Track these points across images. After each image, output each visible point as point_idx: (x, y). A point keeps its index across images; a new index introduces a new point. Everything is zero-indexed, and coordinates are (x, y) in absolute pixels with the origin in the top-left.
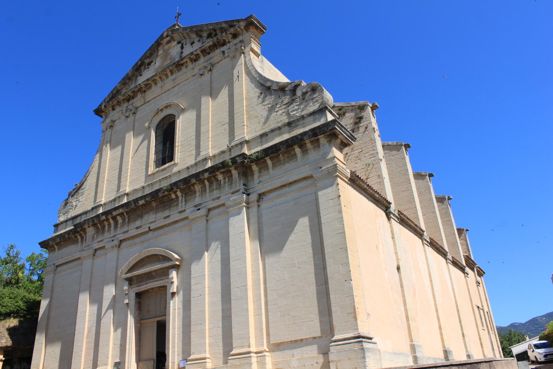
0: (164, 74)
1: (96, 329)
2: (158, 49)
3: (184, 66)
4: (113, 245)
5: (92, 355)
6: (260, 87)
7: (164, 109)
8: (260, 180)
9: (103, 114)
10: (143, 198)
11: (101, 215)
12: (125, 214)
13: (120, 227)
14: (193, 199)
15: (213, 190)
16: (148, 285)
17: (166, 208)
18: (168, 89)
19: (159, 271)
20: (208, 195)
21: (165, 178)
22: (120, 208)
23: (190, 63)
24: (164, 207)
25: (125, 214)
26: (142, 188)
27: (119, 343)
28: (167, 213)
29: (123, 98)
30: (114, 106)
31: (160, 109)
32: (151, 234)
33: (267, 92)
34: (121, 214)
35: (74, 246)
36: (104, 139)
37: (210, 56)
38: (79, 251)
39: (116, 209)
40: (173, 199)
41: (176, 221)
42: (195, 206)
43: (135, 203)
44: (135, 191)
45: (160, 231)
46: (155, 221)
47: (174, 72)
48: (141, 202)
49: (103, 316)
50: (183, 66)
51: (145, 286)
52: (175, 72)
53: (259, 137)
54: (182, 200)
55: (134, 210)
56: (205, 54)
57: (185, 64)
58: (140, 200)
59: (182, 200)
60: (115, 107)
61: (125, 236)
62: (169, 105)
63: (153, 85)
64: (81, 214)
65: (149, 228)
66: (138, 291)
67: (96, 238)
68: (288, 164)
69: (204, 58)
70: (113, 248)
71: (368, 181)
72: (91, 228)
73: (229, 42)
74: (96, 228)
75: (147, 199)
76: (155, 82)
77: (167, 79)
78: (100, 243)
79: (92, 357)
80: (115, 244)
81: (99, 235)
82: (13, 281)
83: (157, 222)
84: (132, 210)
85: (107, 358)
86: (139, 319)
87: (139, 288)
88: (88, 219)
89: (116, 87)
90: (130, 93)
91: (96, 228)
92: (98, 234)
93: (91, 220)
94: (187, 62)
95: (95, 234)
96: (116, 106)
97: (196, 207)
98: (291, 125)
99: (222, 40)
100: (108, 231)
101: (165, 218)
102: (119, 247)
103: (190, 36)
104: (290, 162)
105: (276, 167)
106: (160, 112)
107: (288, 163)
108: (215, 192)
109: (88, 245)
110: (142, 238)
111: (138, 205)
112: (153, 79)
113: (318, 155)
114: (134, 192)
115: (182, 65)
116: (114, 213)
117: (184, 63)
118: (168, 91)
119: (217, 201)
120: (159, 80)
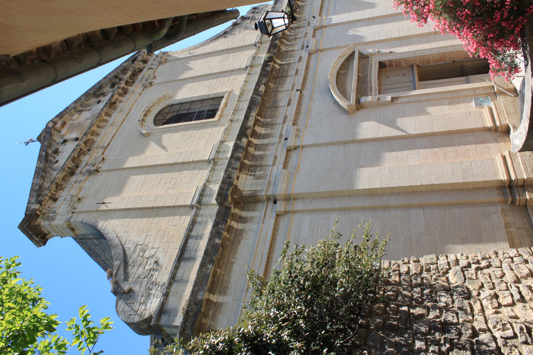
0: (101, 121)
1: (423, 149)
2: (52, 140)
3: (117, 103)
4: (295, 133)
5: (468, 146)
7: (145, 118)
9: (39, 220)
10: (259, 84)
11: (239, 142)
12: (259, 118)
16: (373, 80)
18: (122, 120)
19: (360, 69)
21: (241, 96)
22: (250, 113)
23: (121, 97)
25: (259, 118)
26: (231, 122)
27: (448, 106)
29: (62, 176)
30: (53, 196)
31: (141, 119)
32: (305, 92)
34: (256, 122)
38: (263, 223)
39: (247, 117)
40: (279, 69)
41: (307, 67)
43: (258, 95)
44: (227, 131)
47: (110, 113)
48: (262, 88)
49: (402, 131)
50: (116, 104)
51: (373, 83)
52: (111, 112)
53: (248, 76)
55: (263, 104)
56: (131, 85)
57: (117, 101)
58: (259, 88)
60: (55, 196)
61: (289, 121)
62: (147, 111)
63: (94, 138)
64: (188, 234)
70: (298, 136)
72: (242, 175)
73: (144, 67)
74: (247, 169)
75: (263, 82)
76: (95, 134)
79: (471, 146)
80: (295, 131)
84: (261, 108)
85: (470, 113)
86: (418, 63)
87: (373, 89)
88: (229, 165)
89: (32, 184)
90: (71, 164)
91: (247, 169)
93: (233, 161)
94: (117, 99)
95: (254, 175)
96: (57, 194)
99: (137, 69)
103: (87, 104)
106: (143, 122)
109: (268, 185)
111: (263, 93)
112: (91, 132)
114: (226, 133)
115: (114, 103)
116: (251, 123)
117: (115, 101)
118: (124, 121)
120: (99, 129)
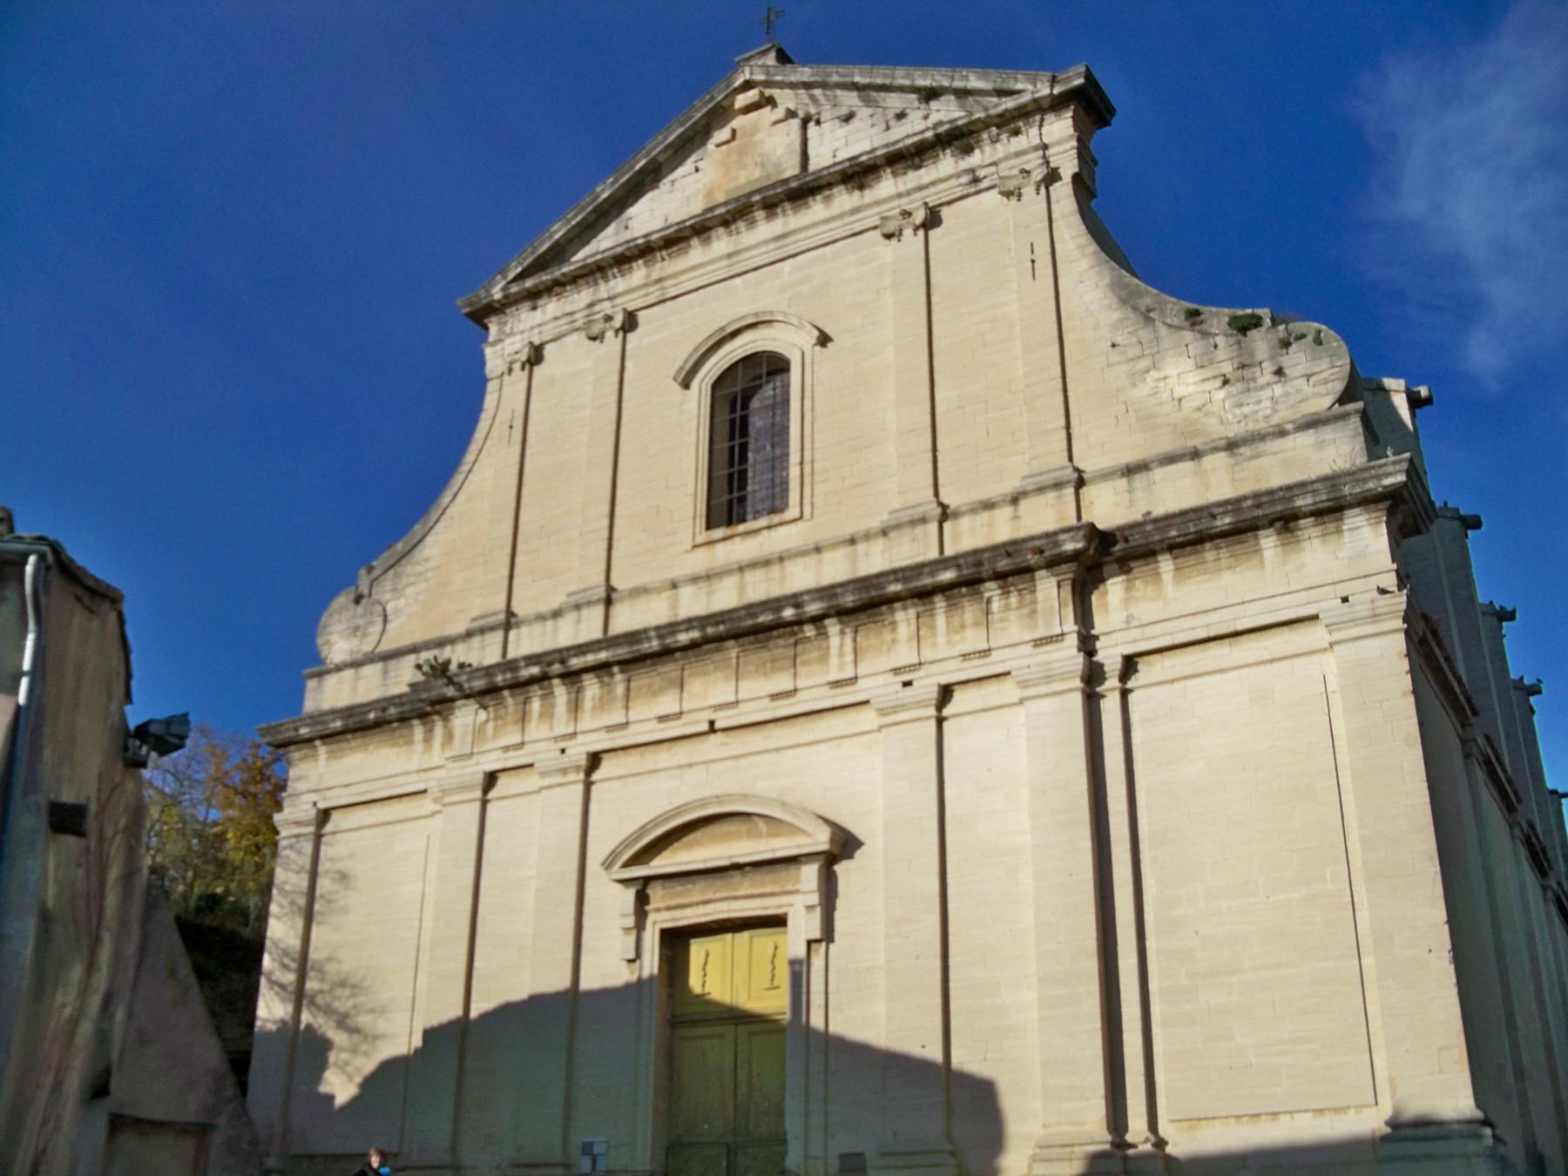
6: (1116, 310)
8: (1130, 612)
11: (522, 664)
13: (594, 708)
14: (885, 648)
15: (963, 627)
17: (778, 664)
20: (941, 638)
24: (773, 661)
28: (783, 682)
33: (1143, 328)
35: (395, 750)
36: (499, 401)
37: (920, 177)
42: (896, 671)
45: (754, 740)
46: (736, 704)
54: (842, 645)
59: (842, 645)
65: (712, 723)
66: (671, 925)
67: (495, 737)
68: (1229, 573)
69: (896, 183)
71: (862, 670)
77: (748, 229)
78: (511, 754)
81: (505, 725)
82: (897, 233)
83: (741, 706)
92: (500, 722)
97: (896, 674)
98: (1236, 451)
100: (541, 716)
101: (775, 697)
102: (1377, 1103)
104: (1238, 569)
105: (1189, 578)
107: (1229, 568)
108: (970, 633)
110: (682, 753)
113: (1337, 558)
119: (976, 662)
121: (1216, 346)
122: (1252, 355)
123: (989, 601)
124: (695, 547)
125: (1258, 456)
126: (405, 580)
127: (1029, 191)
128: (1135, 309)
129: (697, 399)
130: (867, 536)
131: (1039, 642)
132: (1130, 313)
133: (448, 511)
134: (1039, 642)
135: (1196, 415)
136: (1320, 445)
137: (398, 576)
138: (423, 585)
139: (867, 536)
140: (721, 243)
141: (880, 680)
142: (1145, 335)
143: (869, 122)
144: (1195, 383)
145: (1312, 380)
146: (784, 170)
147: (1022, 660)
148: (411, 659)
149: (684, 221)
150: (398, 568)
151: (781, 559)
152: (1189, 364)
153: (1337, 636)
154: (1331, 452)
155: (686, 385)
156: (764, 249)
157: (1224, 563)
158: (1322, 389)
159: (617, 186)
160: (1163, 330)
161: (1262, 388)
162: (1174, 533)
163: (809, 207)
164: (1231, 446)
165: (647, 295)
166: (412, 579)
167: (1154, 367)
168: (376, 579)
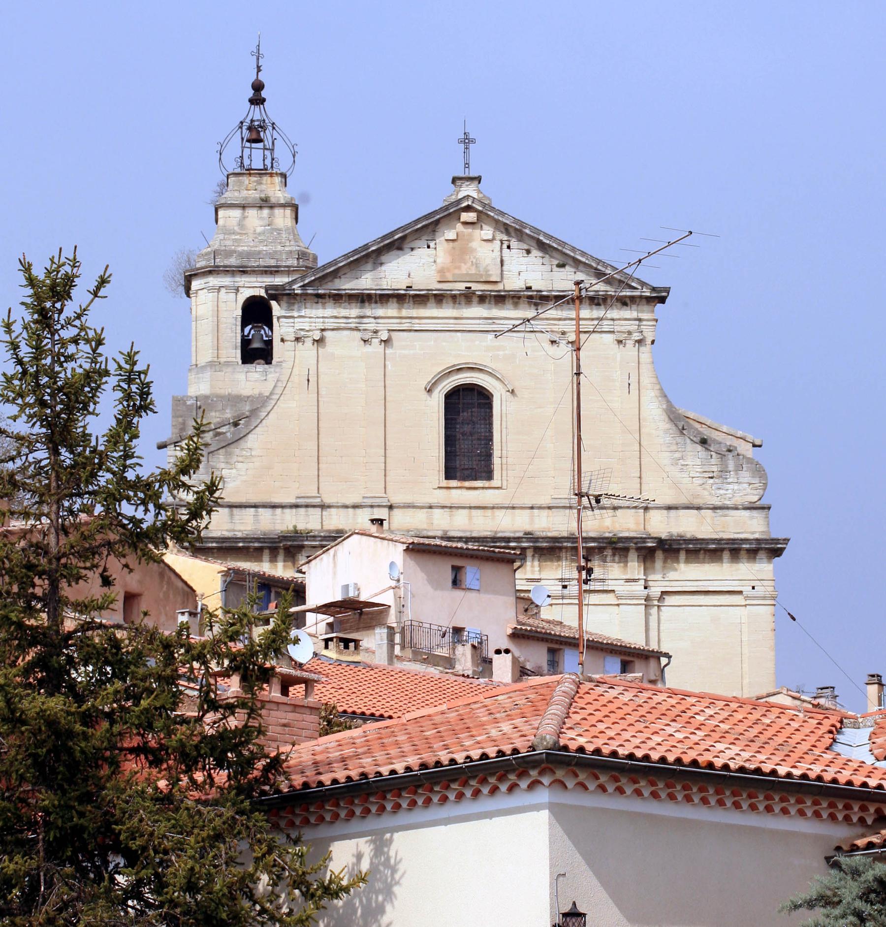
42: (561, 580)
121: (711, 456)
122: (727, 467)
123: (606, 556)
124: (440, 488)
125: (726, 516)
126: (235, 459)
127: (629, 343)
128: (676, 425)
129: (437, 402)
130: (540, 508)
131: (628, 581)
132: (674, 428)
133: (264, 421)
134: (628, 581)
135: (699, 488)
136: (752, 518)
137: (229, 455)
138: (251, 465)
139: (540, 508)
140: (448, 311)
141: (552, 582)
142: (680, 440)
143: (541, 261)
144: (700, 472)
145: (751, 486)
146: (234, 181)
147: (621, 588)
148: (367, 511)
149: (432, 290)
150: (228, 449)
151: (493, 508)
152: (698, 462)
153: (748, 602)
154: (755, 521)
155: (429, 391)
156: (478, 321)
157: (617, 558)
158: (755, 492)
159: (382, 244)
160: (688, 441)
161: (729, 483)
162: (691, 546)
163: (504, 304)
164: (715, 508)
165: (401, 323)
166: (240, 459)
167: (682, 458)
168: (212, 452)
